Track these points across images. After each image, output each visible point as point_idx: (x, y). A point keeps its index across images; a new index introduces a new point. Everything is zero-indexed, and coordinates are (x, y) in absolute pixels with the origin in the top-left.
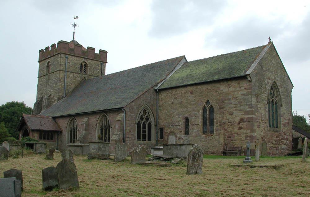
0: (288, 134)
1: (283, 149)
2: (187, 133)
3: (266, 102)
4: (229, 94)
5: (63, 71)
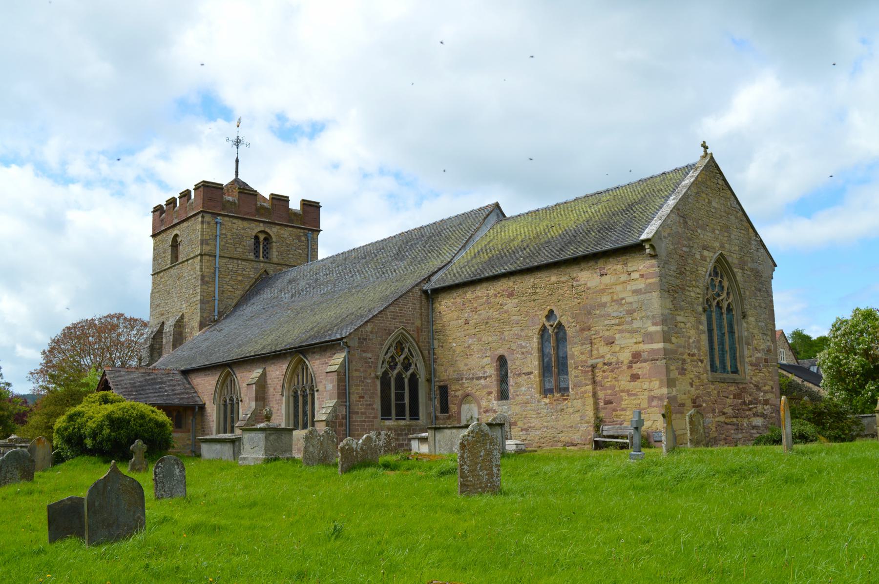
0: (767, 388)
1: (754, 427)
2: (503, 395)
3: (700, 309)
4: (603, 291)
5: (210, 256)
